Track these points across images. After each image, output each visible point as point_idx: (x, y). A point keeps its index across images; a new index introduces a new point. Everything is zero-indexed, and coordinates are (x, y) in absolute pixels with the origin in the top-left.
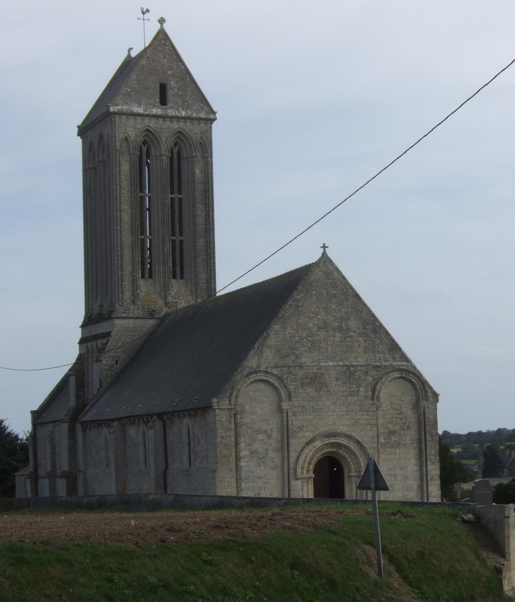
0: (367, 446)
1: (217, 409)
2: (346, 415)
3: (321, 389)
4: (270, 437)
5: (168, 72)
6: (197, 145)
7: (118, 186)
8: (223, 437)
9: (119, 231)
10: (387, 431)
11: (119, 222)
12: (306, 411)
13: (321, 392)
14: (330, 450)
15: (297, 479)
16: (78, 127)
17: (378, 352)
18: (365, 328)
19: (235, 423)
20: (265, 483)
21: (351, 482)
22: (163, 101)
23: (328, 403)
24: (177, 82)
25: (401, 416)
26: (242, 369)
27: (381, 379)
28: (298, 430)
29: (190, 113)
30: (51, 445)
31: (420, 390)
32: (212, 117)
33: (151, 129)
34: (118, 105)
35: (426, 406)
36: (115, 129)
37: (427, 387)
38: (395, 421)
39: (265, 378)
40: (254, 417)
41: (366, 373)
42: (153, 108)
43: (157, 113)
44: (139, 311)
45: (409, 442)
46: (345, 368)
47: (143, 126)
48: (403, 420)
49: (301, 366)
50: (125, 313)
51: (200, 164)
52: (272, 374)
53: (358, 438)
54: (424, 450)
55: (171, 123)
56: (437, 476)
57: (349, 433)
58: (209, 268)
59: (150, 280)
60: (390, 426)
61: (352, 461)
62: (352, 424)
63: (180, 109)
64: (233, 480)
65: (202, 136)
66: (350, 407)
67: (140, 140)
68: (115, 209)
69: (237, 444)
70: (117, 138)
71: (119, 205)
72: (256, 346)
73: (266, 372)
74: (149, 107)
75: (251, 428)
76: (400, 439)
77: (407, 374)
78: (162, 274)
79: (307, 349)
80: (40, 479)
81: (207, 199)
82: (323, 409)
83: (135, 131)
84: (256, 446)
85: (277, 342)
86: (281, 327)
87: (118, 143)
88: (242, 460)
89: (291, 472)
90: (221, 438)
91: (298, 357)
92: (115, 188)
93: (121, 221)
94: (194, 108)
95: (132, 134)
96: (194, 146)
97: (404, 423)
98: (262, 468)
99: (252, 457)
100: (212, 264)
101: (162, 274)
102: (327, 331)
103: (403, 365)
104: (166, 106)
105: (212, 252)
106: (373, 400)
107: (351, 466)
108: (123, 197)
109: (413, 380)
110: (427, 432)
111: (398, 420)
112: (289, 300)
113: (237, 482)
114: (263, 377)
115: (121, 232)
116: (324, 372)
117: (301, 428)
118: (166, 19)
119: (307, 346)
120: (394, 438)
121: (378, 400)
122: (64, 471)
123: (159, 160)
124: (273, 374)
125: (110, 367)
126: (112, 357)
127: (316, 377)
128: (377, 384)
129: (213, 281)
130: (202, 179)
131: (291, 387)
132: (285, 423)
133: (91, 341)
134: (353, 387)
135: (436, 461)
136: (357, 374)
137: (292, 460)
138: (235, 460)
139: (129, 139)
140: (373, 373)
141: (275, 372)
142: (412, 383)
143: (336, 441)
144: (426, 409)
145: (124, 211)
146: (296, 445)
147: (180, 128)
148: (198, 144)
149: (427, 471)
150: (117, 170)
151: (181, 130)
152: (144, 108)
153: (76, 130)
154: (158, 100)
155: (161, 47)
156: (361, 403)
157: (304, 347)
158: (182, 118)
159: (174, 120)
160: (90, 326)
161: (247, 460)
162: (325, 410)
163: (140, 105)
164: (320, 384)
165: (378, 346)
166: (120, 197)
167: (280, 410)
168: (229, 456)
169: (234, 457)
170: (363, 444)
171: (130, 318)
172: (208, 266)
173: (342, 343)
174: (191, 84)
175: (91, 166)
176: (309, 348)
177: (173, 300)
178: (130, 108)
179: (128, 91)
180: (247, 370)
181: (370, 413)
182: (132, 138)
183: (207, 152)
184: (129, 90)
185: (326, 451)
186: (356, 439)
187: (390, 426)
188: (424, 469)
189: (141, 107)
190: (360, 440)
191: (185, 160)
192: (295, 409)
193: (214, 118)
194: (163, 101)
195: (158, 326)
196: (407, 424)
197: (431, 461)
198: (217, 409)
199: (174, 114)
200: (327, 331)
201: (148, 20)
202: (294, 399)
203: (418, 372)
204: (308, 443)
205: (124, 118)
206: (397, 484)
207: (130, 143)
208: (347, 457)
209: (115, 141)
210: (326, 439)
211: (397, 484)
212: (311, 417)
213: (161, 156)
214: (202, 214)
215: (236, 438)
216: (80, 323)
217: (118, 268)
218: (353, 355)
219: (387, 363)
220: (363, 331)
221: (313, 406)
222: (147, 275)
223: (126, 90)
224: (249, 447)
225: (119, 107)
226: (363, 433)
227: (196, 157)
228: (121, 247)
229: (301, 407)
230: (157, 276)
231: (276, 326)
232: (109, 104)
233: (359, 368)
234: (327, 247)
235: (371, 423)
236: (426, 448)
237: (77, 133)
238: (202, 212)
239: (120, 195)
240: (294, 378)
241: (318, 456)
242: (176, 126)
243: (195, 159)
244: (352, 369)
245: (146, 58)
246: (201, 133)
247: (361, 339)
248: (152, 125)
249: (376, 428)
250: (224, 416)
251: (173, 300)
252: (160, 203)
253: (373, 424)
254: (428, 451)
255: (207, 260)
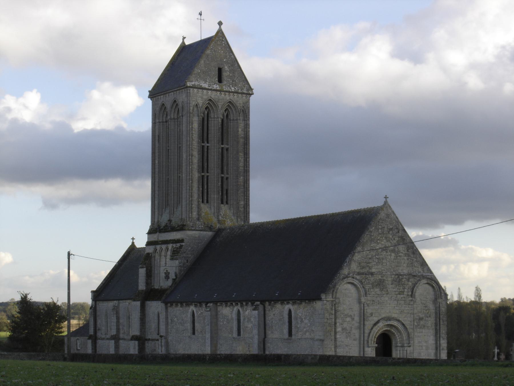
0: (408, 327)
1: (325, 300)
2: (397, 306)
3: (383, 289)
4: (353, 319)
5: (223, 60)
6: (240, 112)
7: (191, 138)
8: (328, 319)
9: (191, 170)
10: (418, 318)
11: (191, 164)
12: (374, 304)
13: (383, 292)
14: (386, 329)
15: (368, 347)
16: (149, 91)
17: (415, 266)
18: (408, 251)
19: (335, 310)
20: (350, 349)
21: (397, 350)
22: (220, 81)
23: (387, 299)
24: (229, 67)
25: (426, 308)
26: (339, 275)
27: (417, 284)
28: (369, 316)
29: (237, 89)
30: (117, 317)
31: (437, 292)
32: (251, 93)
33: (212, 100)
34: (192, 82)
35: (441, 302)
36: (190, 98)
37: (442, 290)
38: (423, 312)
39: (352, 281)
40: (345, 306)
41: (408, 280)
42: (214, 84)
43: (217, 88)
44: (202, 226)
45: (430, 325)
46: (397, 276)
47: (207, 97)
48: (427, 311)
49: (372, 274)
50: (193, 227)
51: (242, 125)
52: (357, 279)
53: (403, 321)
54: (439, 330)
55: (225, 96)
56: (446, 347)
57: (398, 318)
58: (246, 197)
59: (207, 204)
60: (420, 314)
61: (398, 336)
62: (400, 313)
63: (231, 86)
64: (333, 347)
65: (243, 105)
66: (399, 301)
67: (205, 106)
68: (189, 154)
69: (335, 323)
70: (191, 104)
71: (191, 151)
72: (347, 260)
73: (353, 278)
74: (211, 84)
75: (343, 314)
76: (425, 323)
77: (431, 281)
78: (215, 201)
79: (375, 263)
80: (99, 340)
81: (246, 149)
82: (384, 302)
83: (202, 100)
84: (345, 325)
85: (359, 258)
86: (362, 248)
87: (191, 108)
88: (337, 334)
89: (366, 342)
90: (327, 320)
91: (370, 268)
92: (188, 140)
93: (192, 163)
94: (239, 85)
95: (200, 102)
96: (238, 112)
97: (427, 313)
98: (348, 339)
99: (343, 332)
100: (248, 195)
101: (215, 201)
102: (387, 252)
103: (429, 276)
104: (222, 84)
105: (248, 187)
106: (412, 297)
107: (397, 339)
108: (193, 146)
109: (434, 285)
110: (441, 319)
111: (424, 310)
112: (366, 231)
113: (335, 348)
114: (351, 281)
115: (192, 170)
116: (385, 278)
117: (372, 314)
118: (219, 21)
119: (375, 262)
120: (422, 323)
121: (415, 298)
122: (134, 336)
123: (216, 121)
124: (356, 279)
125: (183, 265)
126: (185, 258)
127: (380, 282)
128: (414, 287)
129: (248, 207)
130: (242, 136)
131: (367, 287)
132: (362, 311)
133: (161, 244)
134: (401, 289)
135: (445, 338)
136: (404, 280)
137: (366, 335)
138: (334, 333)
139: (198, 106)
140: (412, 280)
141: (358, 278)
142: (433, 287)
143: (391, 323)
144: (441, 304)
145: (193, 156)
146: (369, 324)
147: (230, 99)
148: (241, 111)
149: (440, 344)
150: (191, 127)
151: (231, 101)
152: (209, 84)
153: (148, 94)
154: (217, 79)
155: (220, 42)
156: (405, 299)
157: (374, 262)
158: (232, 92)
159: (227, 94)
160: (158, 233)
161: (340, 334)
162: (385, 303)
163: (206, 82)
164: (383, 286)
165: (415, 262)
166: (192, 146)
167: (360, 302)
168: (331, 331)
169: (334, 332)
170: (406, 325)
171: (197, 230)
172: (245, 196)
173: (395, 260)
174: (238, 69)
175: (160, 121)
176: (377, 263)
177: (223, 219)
178: (200, 84)
179: (198, 72)
180: (342, 276)
181: (410, 306)
182: (201, 105)
183: (246, 117)
184: (199, 71)
185: (384, 329)
186: (402, 323)
187: (420, 314)
188: (438, 342)
189: (206, 84)
190: (404, 323)
191: (232, 121)
192: (369, 302)
193: (252, 93)
194: (220, 81)
195: (214, 238)
196: (429, 314)
197: (442, 337)
198: (325, 300)
199: (227, 89)
200: (387, 252)
201: (204, 20)
202: (368, 296)
203: (437, 280)
204: (375, 324)
205: (195, 90)
206: (423, 352)
207: (199, 108)
208: (396, 334)
209: (190, 106)
210: (385, 322)
211: (423, 352)
212: (377, 307)
213: (218, 118)
214: (242, 160)
215: (335, 320)
216: (147, 231)
217: (189, 196)
218: (401, 268)
219: (420, 274)
220: (407, 252)
221: (378, 300)
222: (205, 201)
223: (197, 71)
224: (341, 326)
225: (193, 83)
226: (406, 319)
227: (240, 120)
228: (192, 181)
229: (372, 301)
230: (212, 202)
231: (359, 248)
232: (187, 81)
233: (405, 277)
234: (388, 198)
235: (410, 312)
236: (440, 329)
237: (148, 96)
238: (242, 159)
239: (192, 145)
240: (368, 282)
241: (379, 332)
242: (228, 97)
243: (239, 121)
244: (400, 277)
245: (210, 49)
246: (243, 103)
247: (405, 258)
248: (213, 97)
249: (413, 315)
250: (329, 305)
251: (223, 219)
252: (216, 151)
253: (411, 313)
254: (441, 331)
255: (245, 192)
